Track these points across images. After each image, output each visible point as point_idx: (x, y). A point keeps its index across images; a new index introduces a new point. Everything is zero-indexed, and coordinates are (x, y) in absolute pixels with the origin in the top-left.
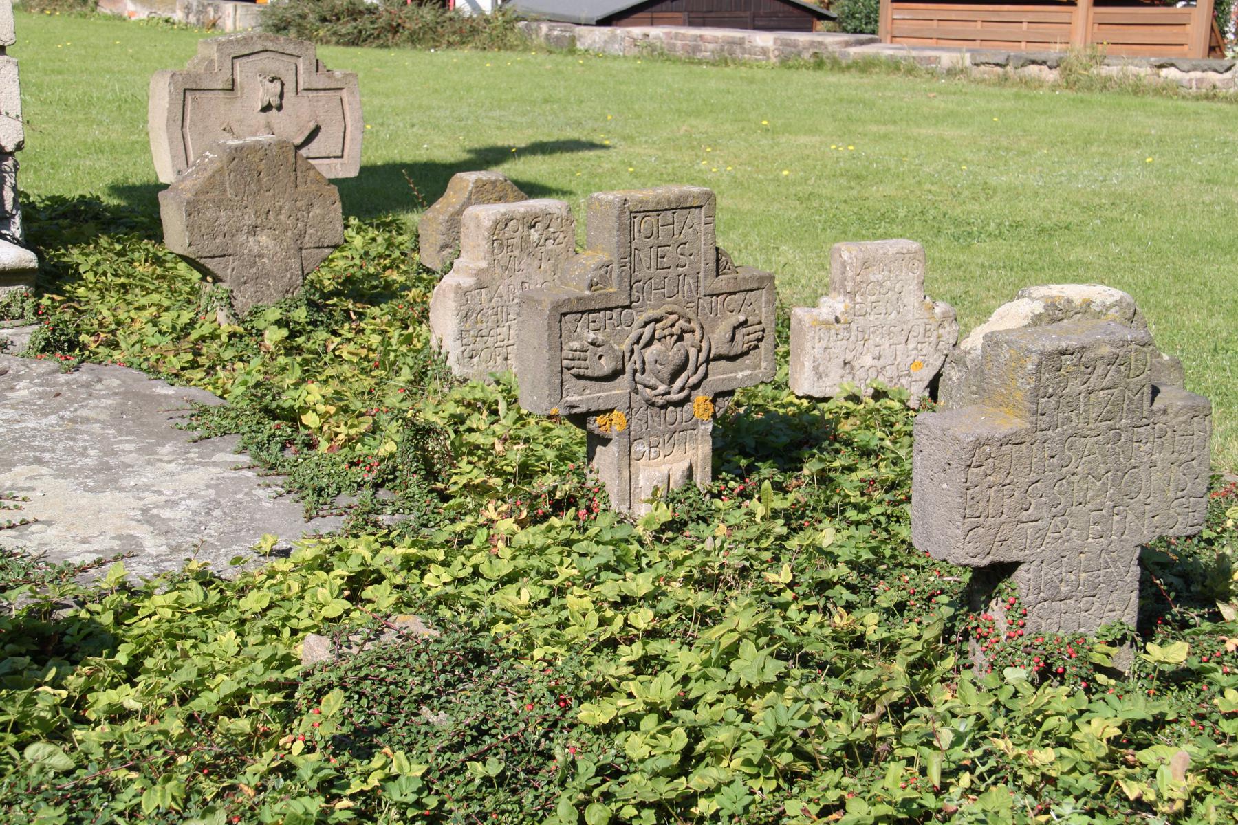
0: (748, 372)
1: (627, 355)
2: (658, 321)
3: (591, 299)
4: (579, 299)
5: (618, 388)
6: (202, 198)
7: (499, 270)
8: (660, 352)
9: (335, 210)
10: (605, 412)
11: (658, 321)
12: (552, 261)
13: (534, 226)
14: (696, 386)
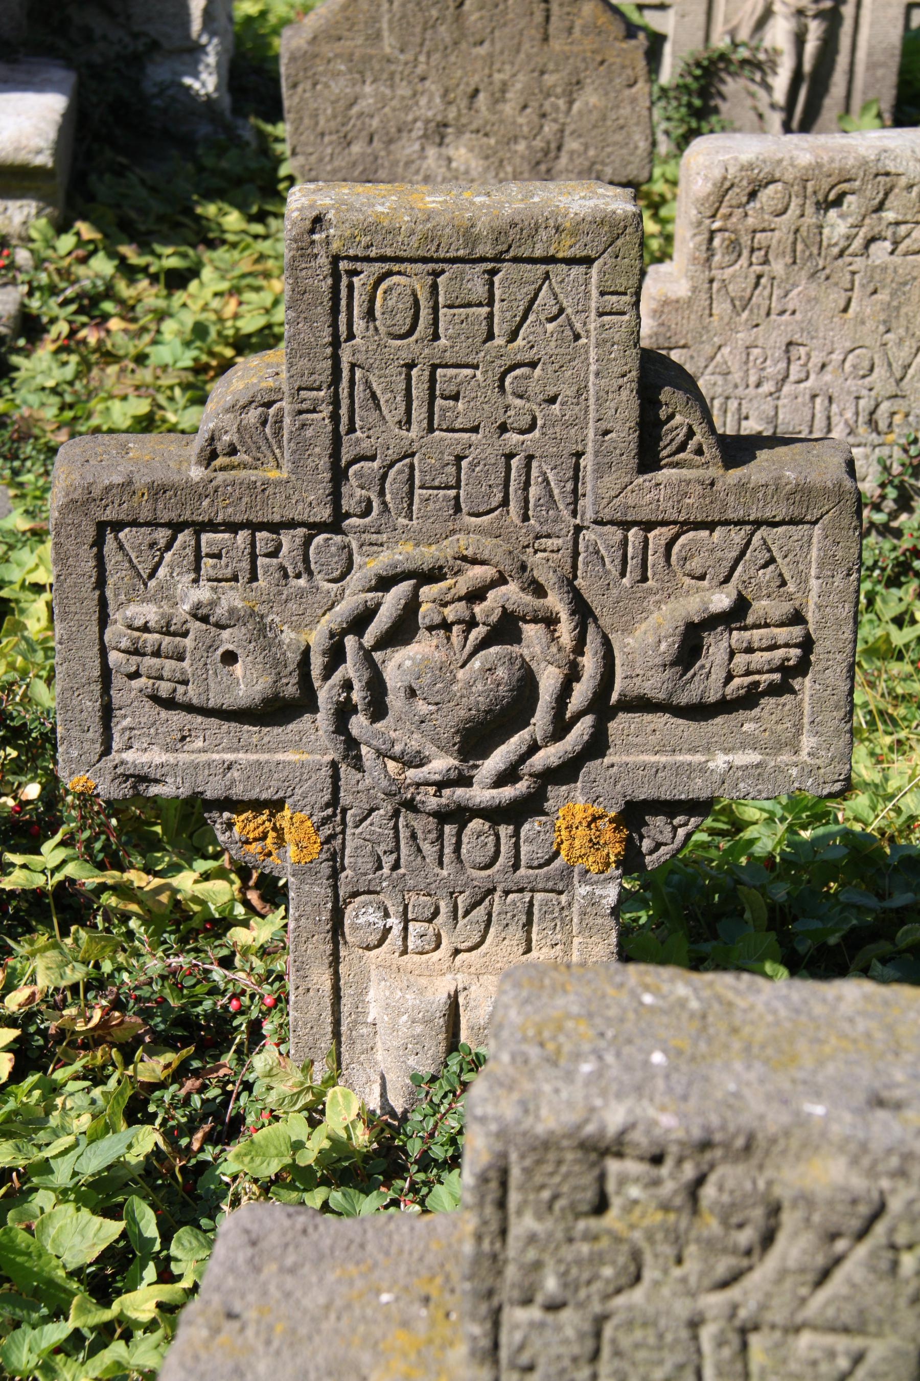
0: (754, 757)
1: (317, 663)
2: (433, 575)
3: (198, 492)
4: (158, 491)
5: (297, 745)
6: (327, 50)
7: (721, 307)
8: (424, 664)
9: (634, 100)
10: (257, 806)
11: (433, 575)
12: (883, 296)
13: (838, 202)
14: (565, 773)
